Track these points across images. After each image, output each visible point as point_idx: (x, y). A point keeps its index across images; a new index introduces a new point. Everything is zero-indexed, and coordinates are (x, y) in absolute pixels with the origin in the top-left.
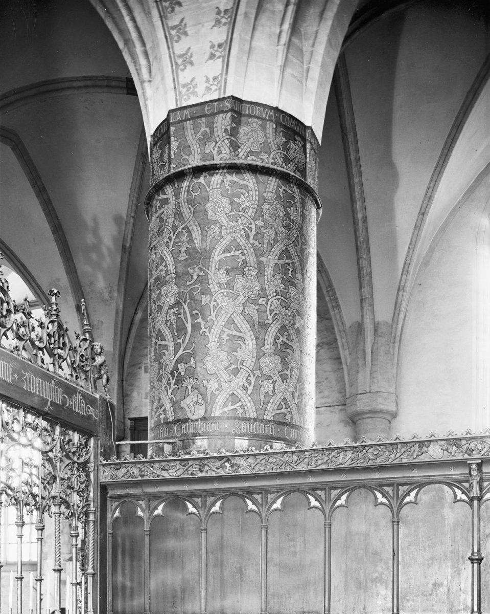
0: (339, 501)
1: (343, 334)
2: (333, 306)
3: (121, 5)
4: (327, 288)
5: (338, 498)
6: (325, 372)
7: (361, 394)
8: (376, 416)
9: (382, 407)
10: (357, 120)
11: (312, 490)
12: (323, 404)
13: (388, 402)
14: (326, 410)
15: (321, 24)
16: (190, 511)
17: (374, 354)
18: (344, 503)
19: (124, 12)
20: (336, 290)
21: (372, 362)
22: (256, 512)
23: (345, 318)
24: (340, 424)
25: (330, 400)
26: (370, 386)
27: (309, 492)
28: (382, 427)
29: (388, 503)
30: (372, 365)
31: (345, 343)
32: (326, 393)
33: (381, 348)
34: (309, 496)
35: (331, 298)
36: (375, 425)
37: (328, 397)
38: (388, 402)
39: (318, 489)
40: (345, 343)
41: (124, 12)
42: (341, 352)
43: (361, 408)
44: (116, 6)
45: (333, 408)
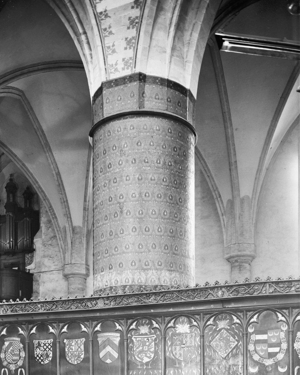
0: (252, 319)
1: (59, 233)
2: (53, 218)
3: (68, 5)
4: (49, 208)
5: (252, 317)
6: (56, 251)
7: (67, 264)
8: (75, 276)
9: (77, 271)
10: (223, 63)
11: (281, 309)
12: (55, 269)
13: (81, 269)
14: (56, 273)
15: (198, 12)
16: (83, 330)
17: (73, 243)
18: (212, 323)
19: (71, 9)
20: (54, 209)
21: (72, 247)
22: (86, 332)
23: (60, 224)
24: (63, 280)
25: (58, 267)
26: (71, 261)
27: (233, 313)
28: (79, 282)
29: (197, 324)
30: (72, 249)
31: (61, 238)
32: (56, 263)
33: (77, 240)
34: (152, 321)
35: (52, 213)
36: (75, 281)
37: (57, 265)
38: (81, 269)
39: (196, 315)
40: (61, 238)
41: (71, 9)
42: (59, 242)
43: (67, 272)
44: (65, 5)
45: (59, 271)
